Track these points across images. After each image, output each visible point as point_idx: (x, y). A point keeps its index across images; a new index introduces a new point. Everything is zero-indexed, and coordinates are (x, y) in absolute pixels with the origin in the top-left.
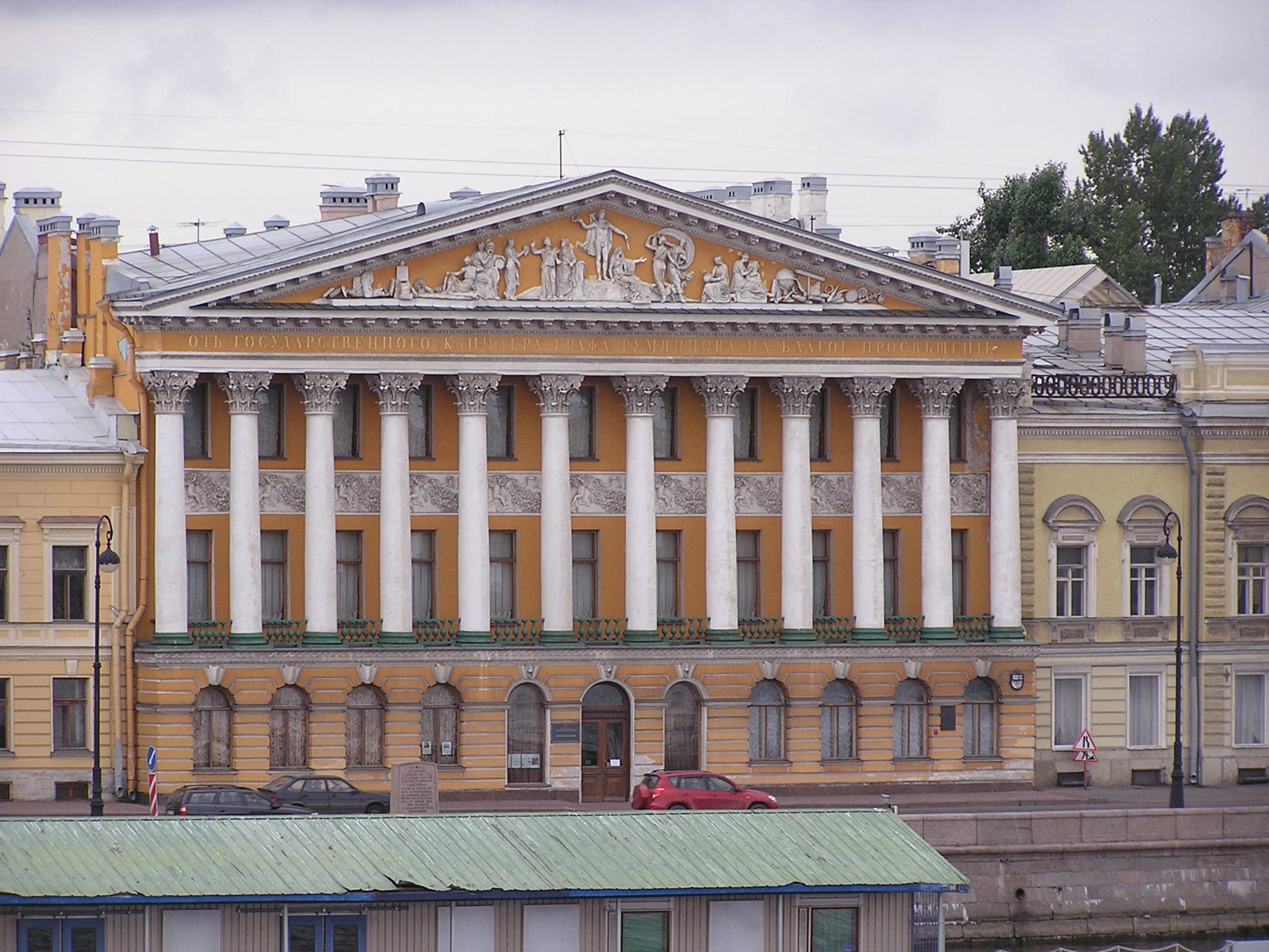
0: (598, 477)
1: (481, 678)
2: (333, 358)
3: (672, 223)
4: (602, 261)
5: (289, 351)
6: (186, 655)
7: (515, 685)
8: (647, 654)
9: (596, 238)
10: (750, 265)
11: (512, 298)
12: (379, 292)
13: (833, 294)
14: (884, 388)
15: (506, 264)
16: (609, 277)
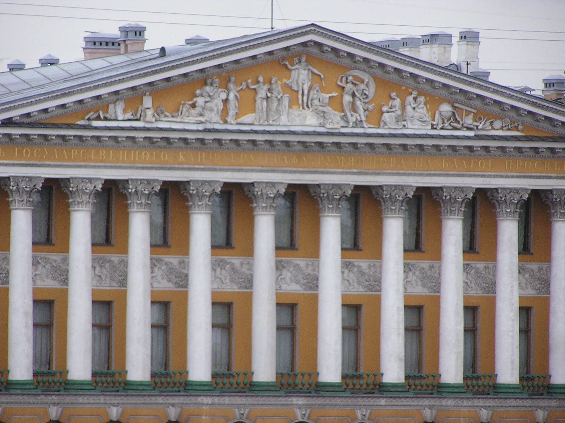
1: (204, 417)
2: (92, 167)
3: (358, 65)
5: (58, 160)
9: (298, 77)
10: (419, 99)
11: (233, 122)
12: (129, 115)
14: (521, 197)
15: (228, 96)
16: (308, 107)
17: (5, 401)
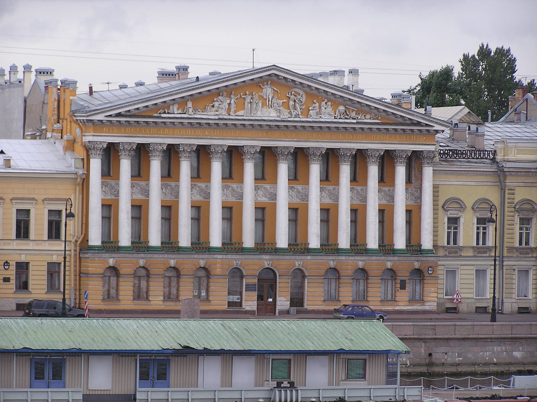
0: (266, 186)
3: (297, 86)
4: (269, 101)
6: (101, 254)
7: (231, 268)
8: (284, 257)
9: (267, 92)
10: (328, 103)
11: (233, 115)
12: (180, 111)
13: (360, 116)
15: (231, 101)
16: (271, 107)
17: (117, 256)
